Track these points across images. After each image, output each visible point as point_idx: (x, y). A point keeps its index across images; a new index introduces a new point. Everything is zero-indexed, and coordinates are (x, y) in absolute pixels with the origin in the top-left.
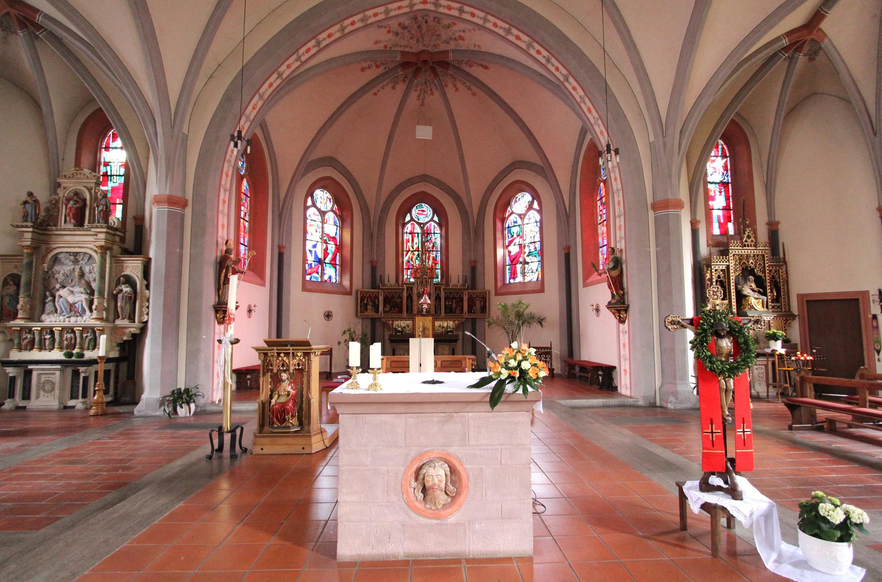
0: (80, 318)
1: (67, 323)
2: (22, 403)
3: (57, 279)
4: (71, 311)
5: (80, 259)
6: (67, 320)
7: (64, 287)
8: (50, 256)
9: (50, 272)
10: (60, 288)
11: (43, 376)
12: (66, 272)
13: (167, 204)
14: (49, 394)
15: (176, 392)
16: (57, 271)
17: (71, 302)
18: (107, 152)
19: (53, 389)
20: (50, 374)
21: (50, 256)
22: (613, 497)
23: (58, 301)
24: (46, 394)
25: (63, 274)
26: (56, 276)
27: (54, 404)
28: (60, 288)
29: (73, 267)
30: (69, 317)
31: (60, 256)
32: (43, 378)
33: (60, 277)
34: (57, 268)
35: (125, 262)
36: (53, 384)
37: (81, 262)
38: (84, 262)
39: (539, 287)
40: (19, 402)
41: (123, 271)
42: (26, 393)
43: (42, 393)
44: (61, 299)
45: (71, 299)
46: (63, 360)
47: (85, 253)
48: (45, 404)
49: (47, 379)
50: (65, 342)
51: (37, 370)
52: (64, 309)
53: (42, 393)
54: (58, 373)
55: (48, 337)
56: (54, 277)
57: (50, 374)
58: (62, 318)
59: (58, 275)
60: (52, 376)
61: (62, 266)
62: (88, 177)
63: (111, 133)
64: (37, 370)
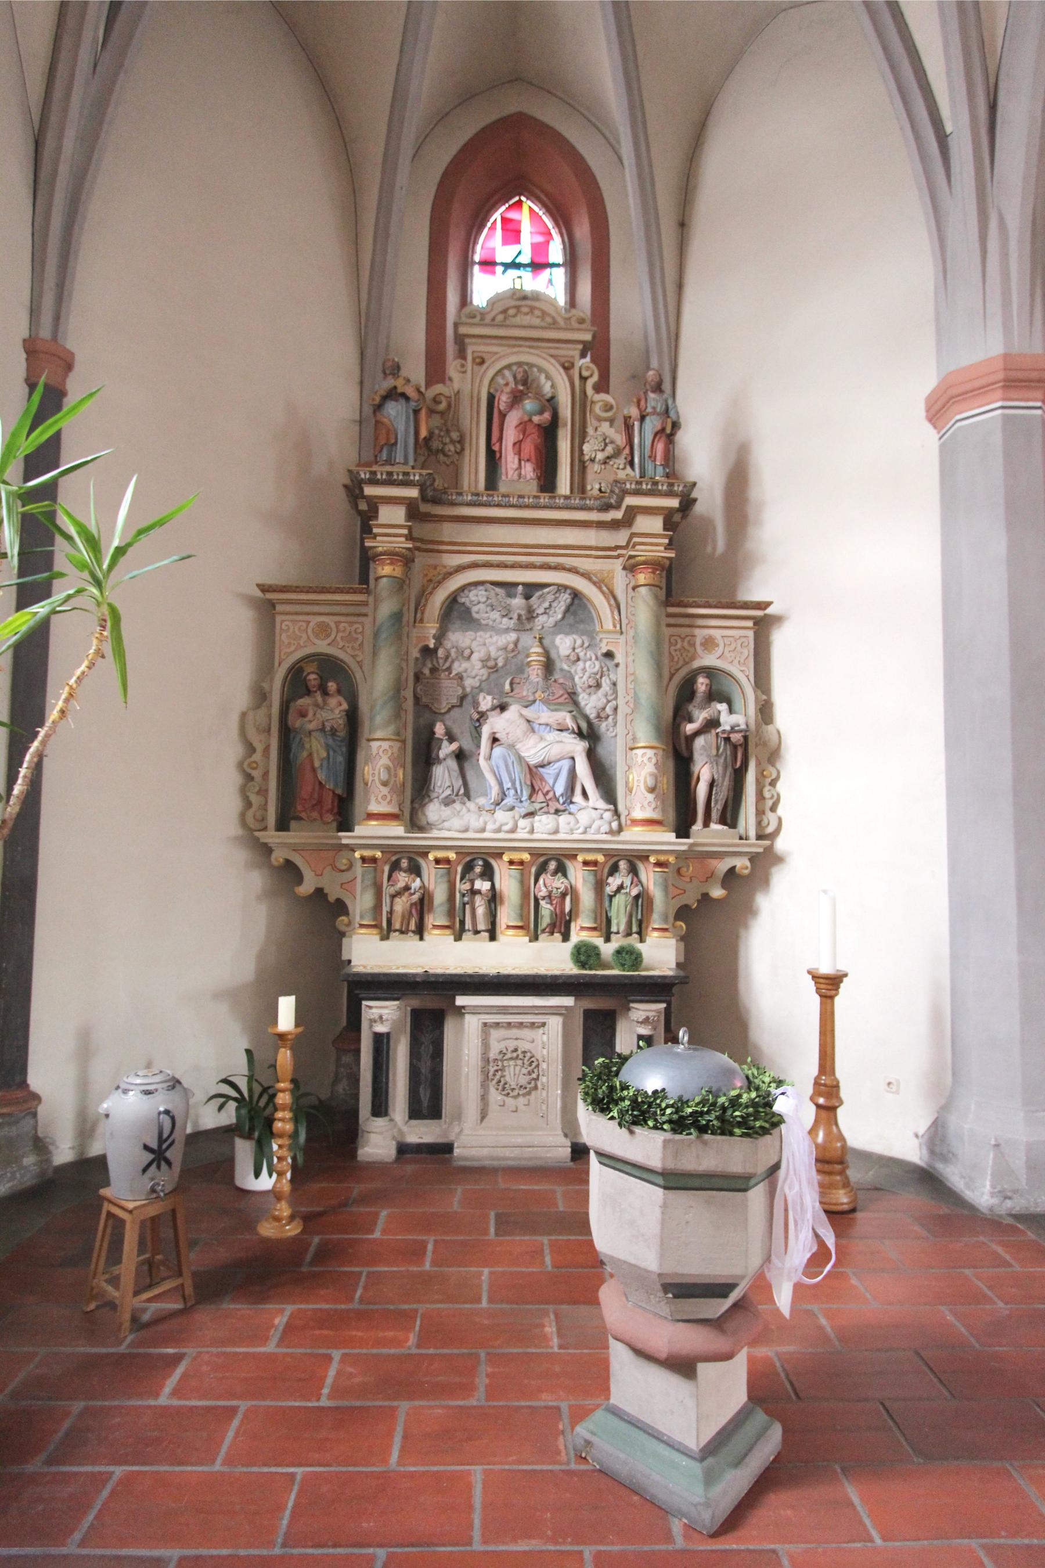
0: (563, 819)
1: (521, 834)
2: (422, 1133)
3: (460, 677)
4: (533, 790)
5: (541, 610)
6: (523, 823)
7: (503, 708)
8: (440, 596)
9: (441, 653)
10: (493, 709)
11: (495, 1034)
12: (493, 654)
13: (999, 394)
14: (522, 1100)
15: (821, 1101)
16: (460, 652)
17: (533, 761)
18: (488, 277)
19: (531, 1087)
20: (521, 1025)
21: (440, 596)
22: (1001, 1349)
23: (489, 758)
24: (509, 1101)
25: (484, 661)
26: (458, 667)
27: (550, 1140)
28: (493, 709)
29: (513, 636)
30: (531, 814)
31: (475, 598)
32: (498, 1042)
33: (473, 671)
34: (458, 638)
35: (701, 622)
36: (532, 1063)
37: (542, 619)
38: (551, 621)
39: (655, 929)
40: (405, 1129)
41: (693, 658)
42: (425, 1095)
43: (495, 1096)
44: (498, 751)
45: (533, 751)
46: (571, 977)
47: (562, 588)
48: (519, 1141)
49: (512, 1045)
50: (546, 908)
51: (476, 1010)
52: (507, 784)
53: (495, 1096)
54: (555, 1023)
55: (483, 885)
56: (449, 669)
57: (521, 1025)
58: (502, 816)
59: (465, 665)
60: (527, 1033)
61: (476, 631)
62: (555, 322)
63: (497, 216)
64: (476, 1010)
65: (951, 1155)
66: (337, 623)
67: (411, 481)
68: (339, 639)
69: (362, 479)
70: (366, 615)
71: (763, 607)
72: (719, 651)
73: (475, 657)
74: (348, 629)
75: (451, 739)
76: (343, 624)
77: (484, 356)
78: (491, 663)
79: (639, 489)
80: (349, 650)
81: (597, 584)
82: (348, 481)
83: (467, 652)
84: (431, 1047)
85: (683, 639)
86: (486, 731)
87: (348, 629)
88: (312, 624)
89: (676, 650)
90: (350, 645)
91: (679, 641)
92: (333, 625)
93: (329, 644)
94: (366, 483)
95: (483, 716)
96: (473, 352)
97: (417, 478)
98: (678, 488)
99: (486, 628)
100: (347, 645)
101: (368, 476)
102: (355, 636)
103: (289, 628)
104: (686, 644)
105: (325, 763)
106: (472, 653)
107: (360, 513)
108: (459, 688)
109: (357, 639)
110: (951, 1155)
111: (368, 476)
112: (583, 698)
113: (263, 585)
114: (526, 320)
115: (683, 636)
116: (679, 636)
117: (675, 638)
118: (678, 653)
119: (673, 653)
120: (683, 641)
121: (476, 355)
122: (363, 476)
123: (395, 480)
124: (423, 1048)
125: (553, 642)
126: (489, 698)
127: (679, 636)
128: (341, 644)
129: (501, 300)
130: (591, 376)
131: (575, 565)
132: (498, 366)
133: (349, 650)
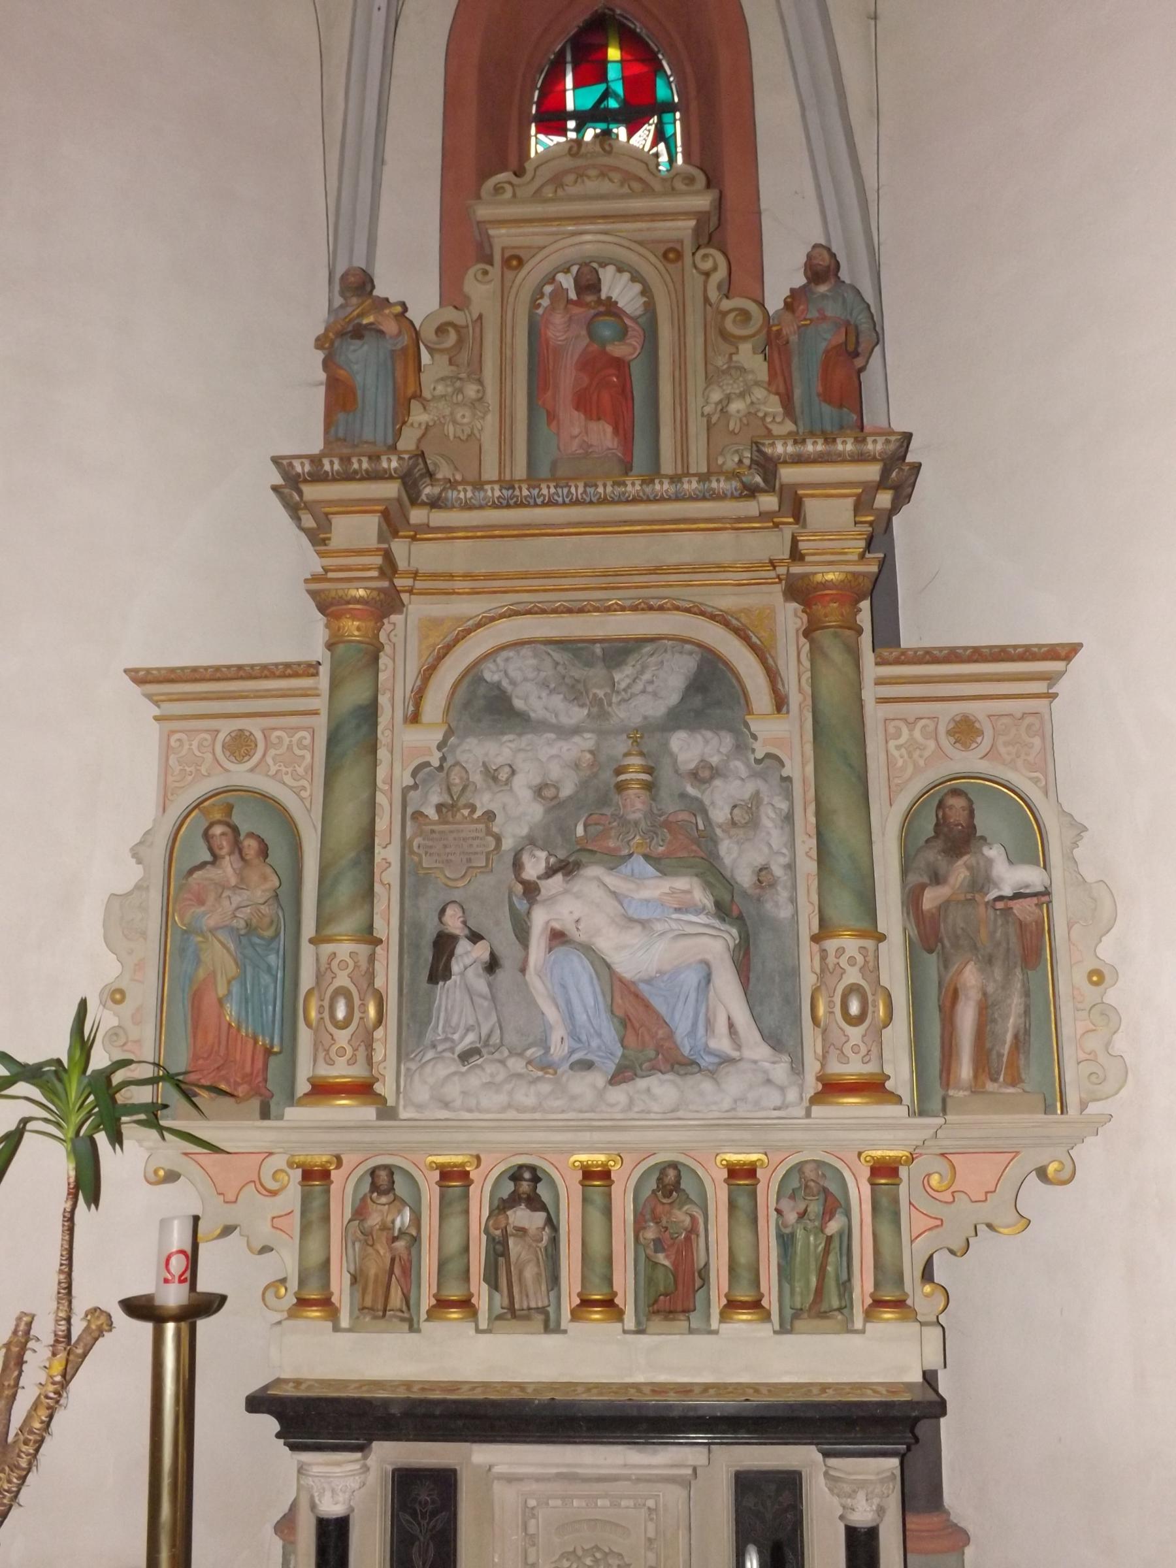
10: (550, 872)
16: (491, 776)
28: (550, 872)
65: (777, 1059)
66: (265, 732)
67: (385, 471)
68: (269, 760)
69: (298, 475)
70: (315, 713)
71: (1063, 654)
72: (986, 743)
73: (519, 782)
74: (287, 740)
75: (475, 937)
76: (278, 733)
77: (521, 253)
78: (549, 793)
79: (829, 453)
80: (288, 779)
81: (741, 633)
82: (278, 480)
83: (503, 775)
84: (431, 1545)
85: (911, 725)
86: (540, 919)
87: (287, 740)
88: (221, 736)
89: (898, 747)
90: (290, 770)
91: (905, 730)
92: (259, 736)
93: (252, 770)
94: (305, 481)
95: (531, 890)
96: (503, 249)
97: (394, 464)
98: (874, 446)
99: (541, 726)
100: (284, 769)
101: (307, 468)
102: (298, 752)
103: (182, 745)
104: (917, 734)
105: (235, 988)
106: (513, 772)
107: (306, 531)
108: (490, 839)
109: (303, 757)
110: (777, 1059)
111: (307, 468)
112: (728, 850)
113: (136, 671)
114: (592, 186)
115: (911, 720)
116: (905, 720)
117: (897, 723)
118: (903, 750)
119: (896, 753)
120: (911, 730)
121: (507, 255)
122: (299, 469)
123: (355, 472)
124: (415, 1549)
125: (665, 745)
126: (542, 855)
127: (905, 720)
128: (273, 769)
129: (553, 159)
130: (715, 269)
131: (697, 599)
132: (546, 267)
133: (288, 779)
